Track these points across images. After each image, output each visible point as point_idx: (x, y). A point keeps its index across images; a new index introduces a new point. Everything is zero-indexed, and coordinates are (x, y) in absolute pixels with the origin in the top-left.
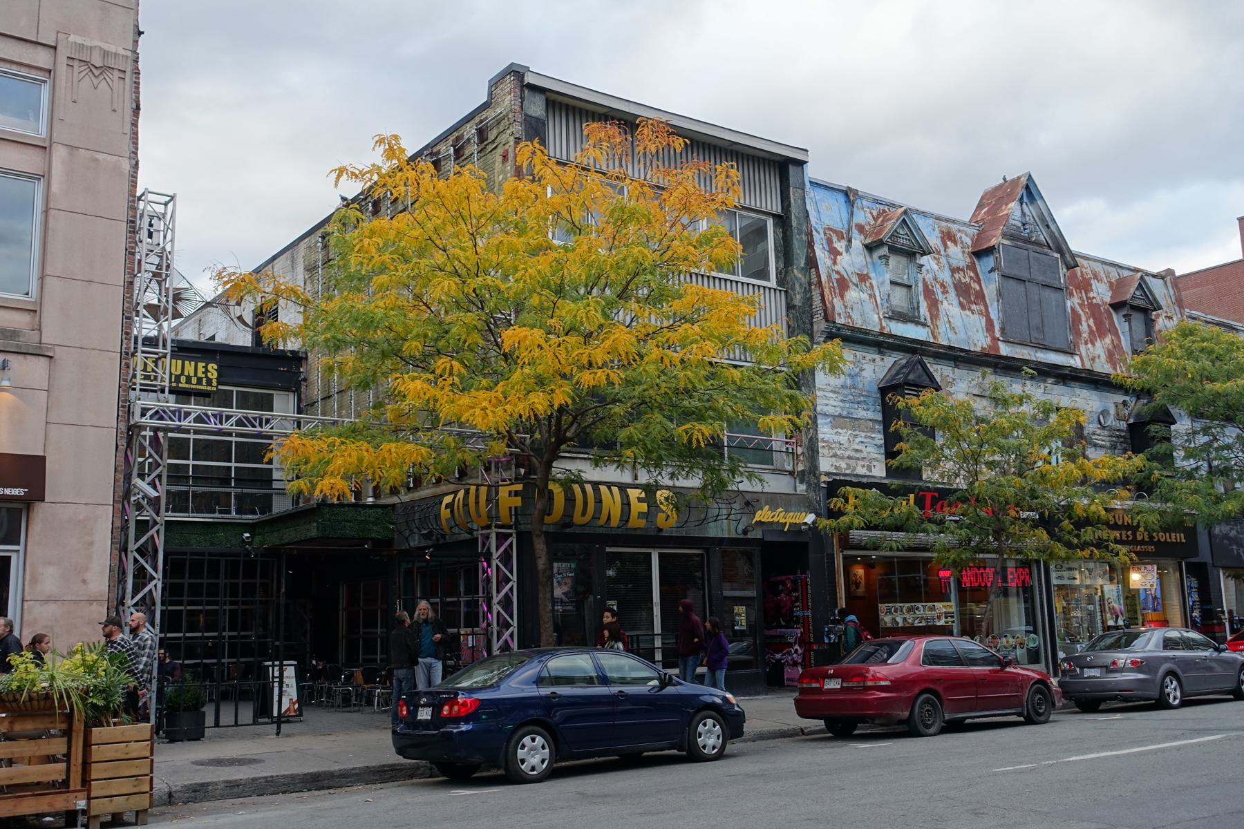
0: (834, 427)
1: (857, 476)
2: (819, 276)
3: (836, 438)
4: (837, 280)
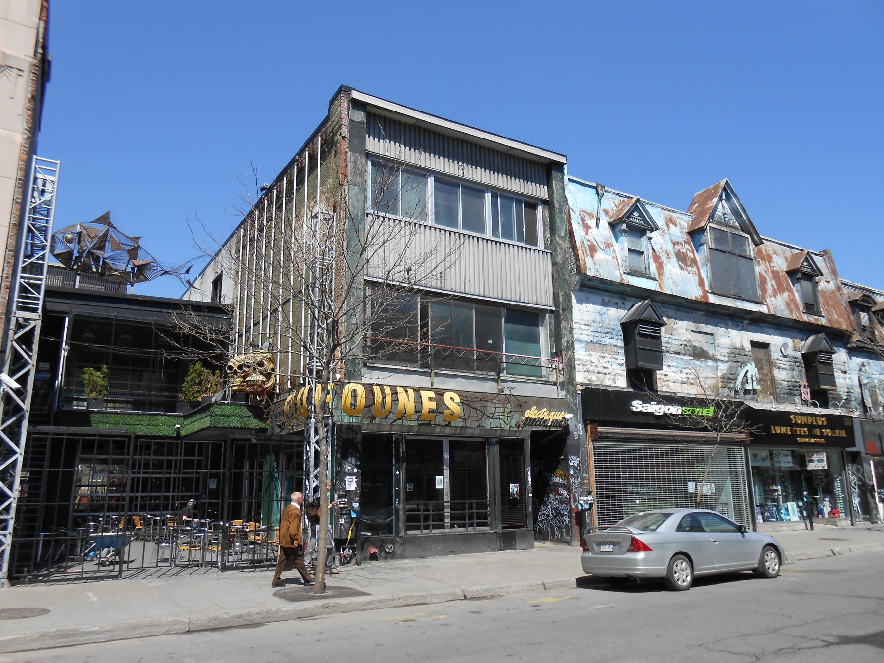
3: (589, 358)
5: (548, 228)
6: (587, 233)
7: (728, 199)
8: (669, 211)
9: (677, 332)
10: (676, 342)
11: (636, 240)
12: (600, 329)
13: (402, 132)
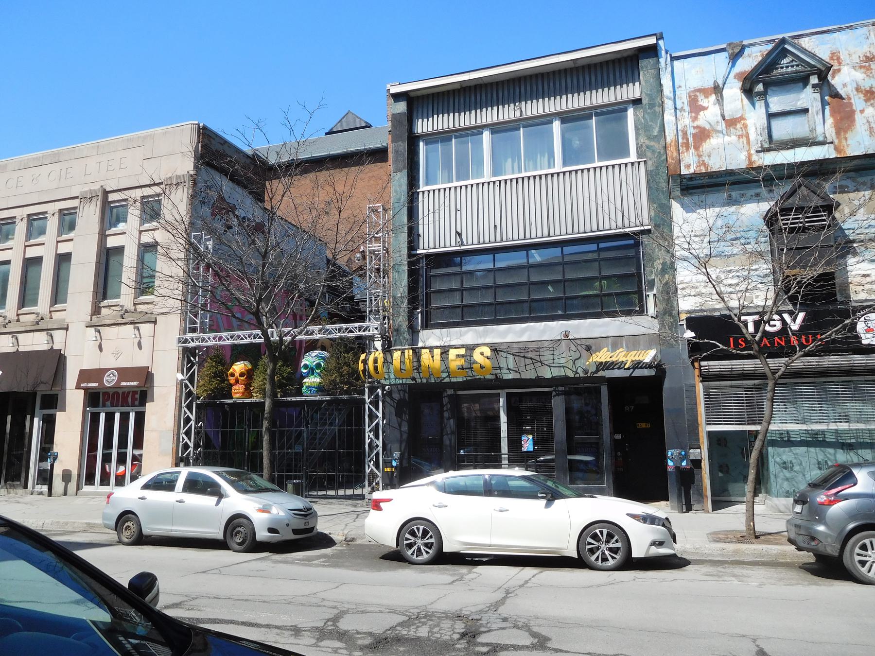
6: (695, 119)
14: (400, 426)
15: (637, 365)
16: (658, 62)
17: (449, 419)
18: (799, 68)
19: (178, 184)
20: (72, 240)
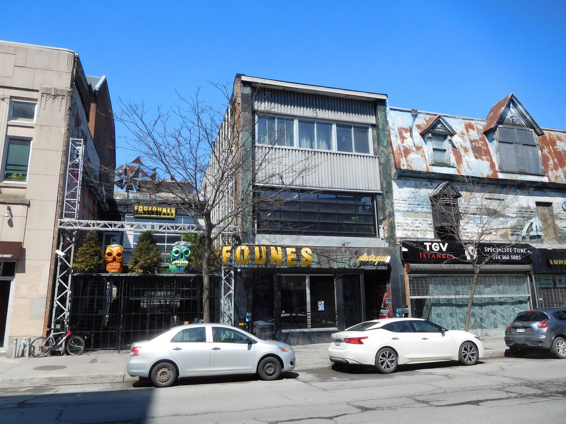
0: (404, 216)
1: (418, 238)
2: (392, 149)
3: (405, 221)
4: (404, 150)
5: (376, 142)
6: (403, 142)
7: (515, 106)
8: (469, 120)
9: (470, 201)
10: (474, 207)
11: (440, 142)
12: (413, 203)
13: (276, 96)
14: (247, 295)
15: (380, 264)
16: (386, 109)
17: (277, 291)
18: (444, 131)
19: (55, 96)
20: (33, 127)
